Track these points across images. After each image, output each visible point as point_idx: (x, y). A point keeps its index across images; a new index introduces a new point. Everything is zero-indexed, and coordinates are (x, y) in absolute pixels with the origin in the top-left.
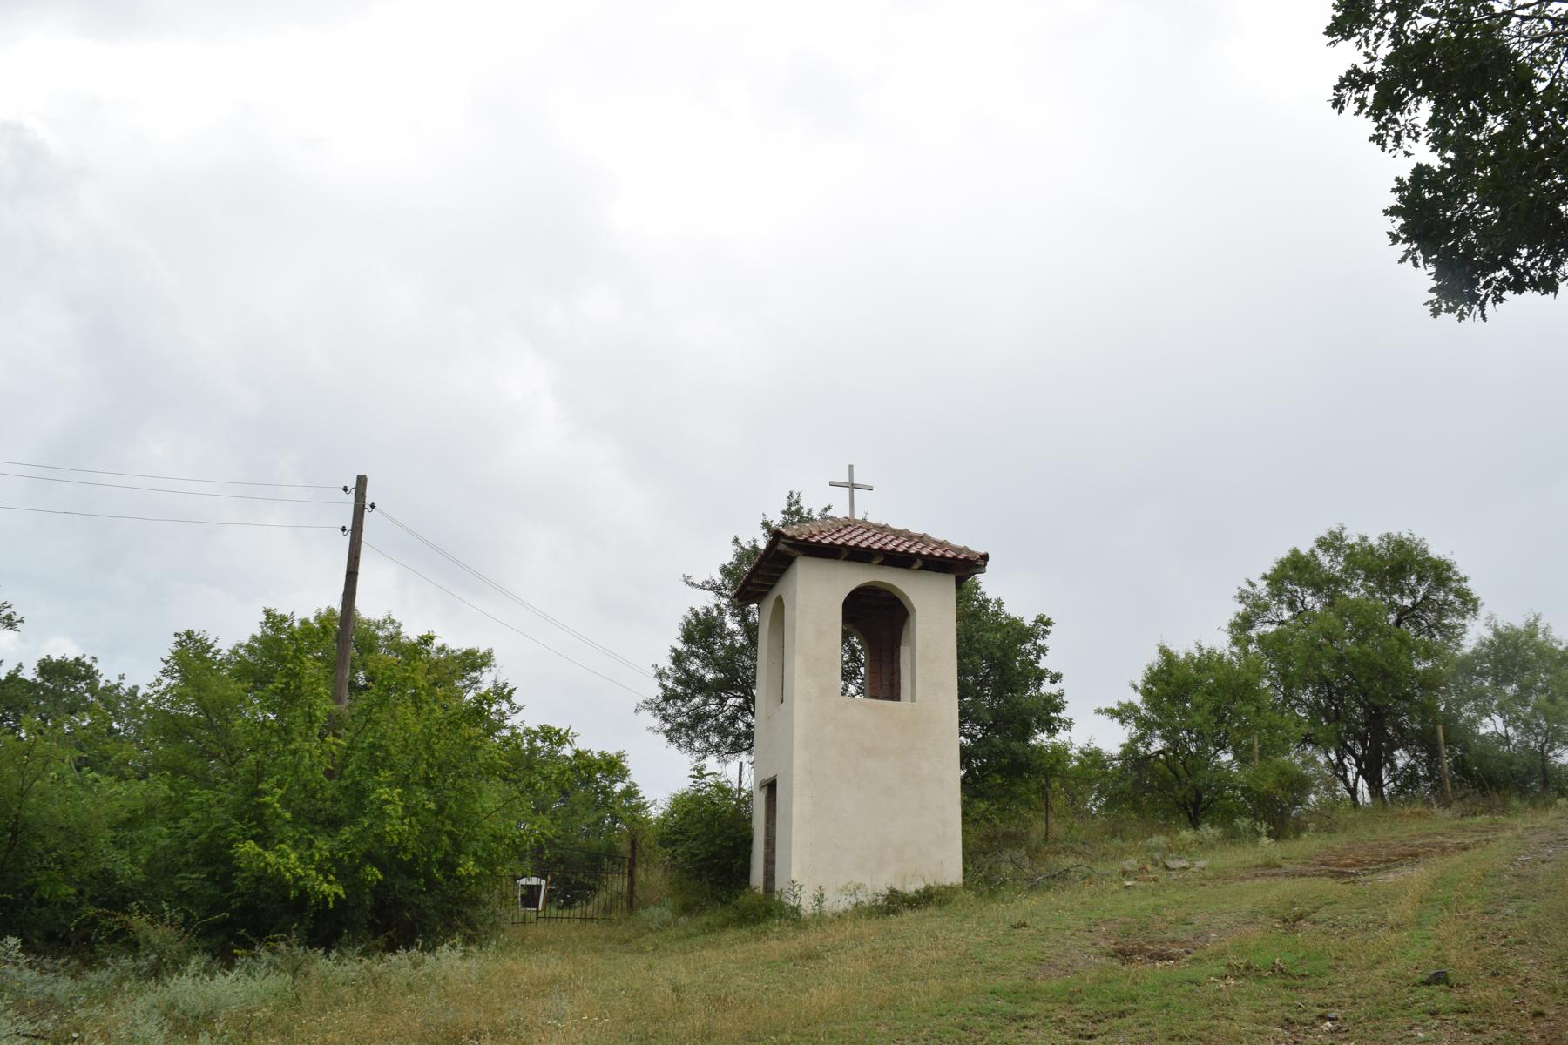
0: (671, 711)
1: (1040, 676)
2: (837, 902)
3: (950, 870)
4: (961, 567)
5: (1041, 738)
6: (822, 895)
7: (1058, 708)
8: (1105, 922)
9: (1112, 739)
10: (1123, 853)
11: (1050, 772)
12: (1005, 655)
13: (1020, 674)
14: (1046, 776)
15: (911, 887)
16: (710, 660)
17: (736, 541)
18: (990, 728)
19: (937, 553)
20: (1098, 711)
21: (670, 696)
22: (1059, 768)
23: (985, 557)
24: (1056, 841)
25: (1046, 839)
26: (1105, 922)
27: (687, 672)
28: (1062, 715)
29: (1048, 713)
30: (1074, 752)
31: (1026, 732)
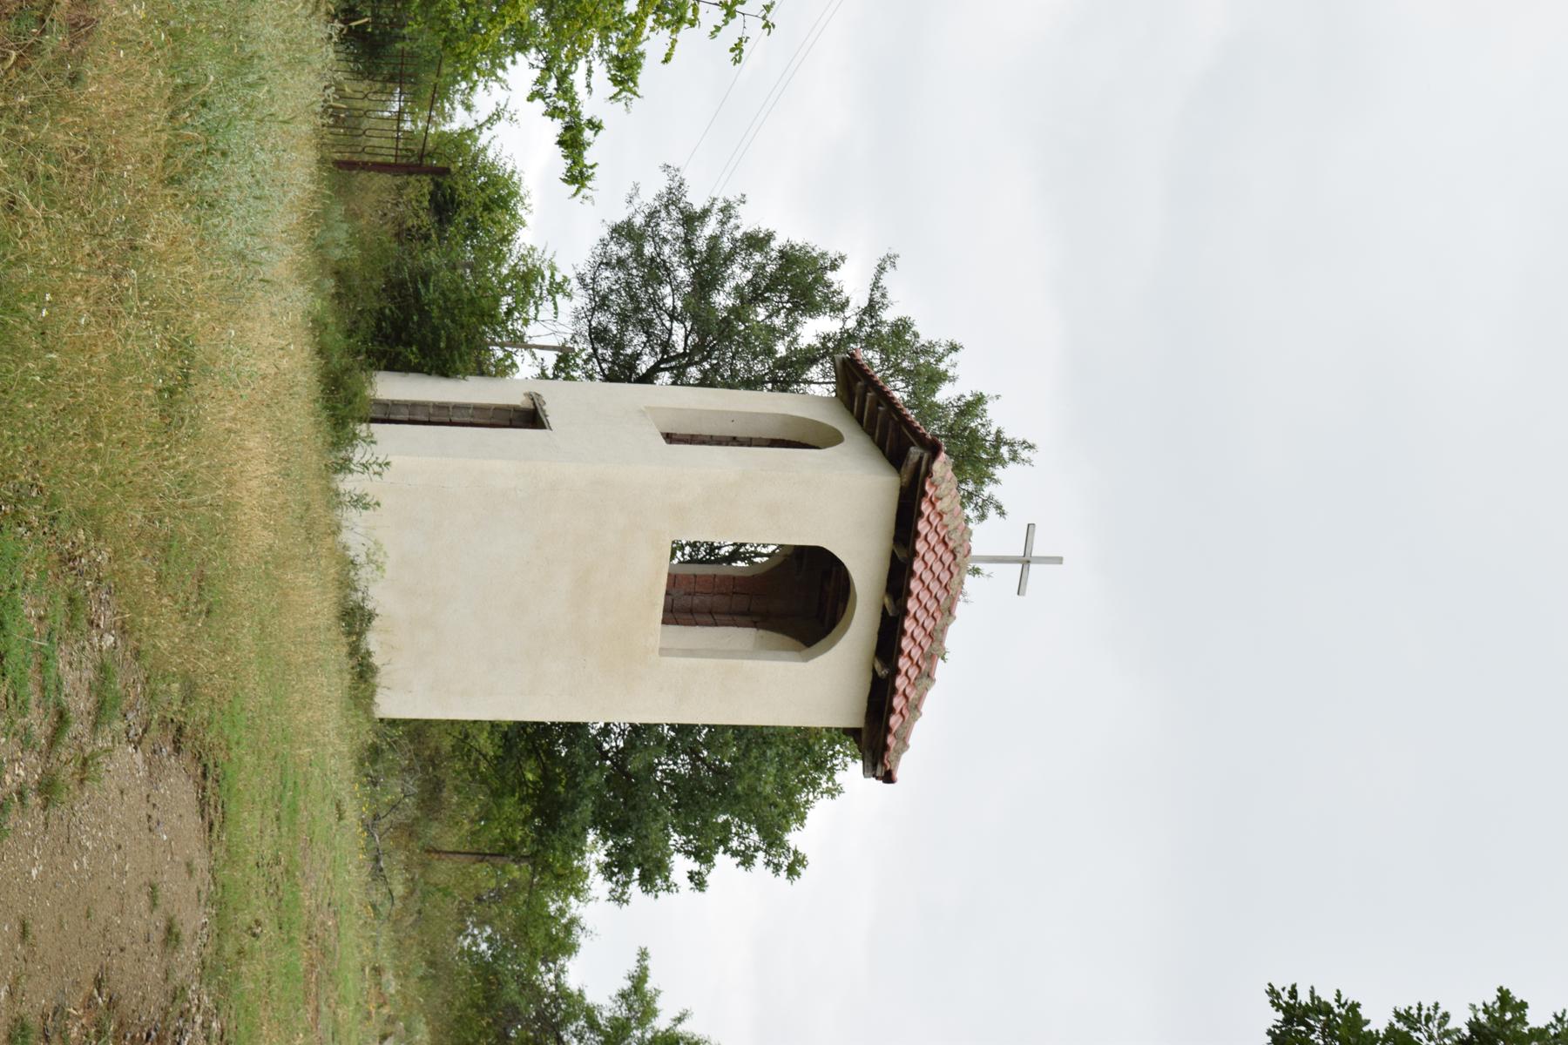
0: (665, 228)
1: (703, 855)
2: (357, 532)
3: (393, 703)
4: (876, 739)
5: (596, 852)
6: (366, 507)
7: (646, 881)
8: (337, 927)
9: (592, 974)
10: (403, 975)
11: (538, 861)
12: (737, 797)
13: (705, 822)
14: (534, 855)
15: (373, 641)
16: (751, 296)
17: (954, 348)
18: (620, 766)
19: (898, 702)
20: (644, 955)
21: (691, 220)
22: (548, 878)
23: (888, 778)
24: (425, 865)
25: (429, 851)
26: (337, 927)
27: (729, 258)
28: (634, 888)
29: (639, 864)
30: (575, 907)
31: (612, 827)
